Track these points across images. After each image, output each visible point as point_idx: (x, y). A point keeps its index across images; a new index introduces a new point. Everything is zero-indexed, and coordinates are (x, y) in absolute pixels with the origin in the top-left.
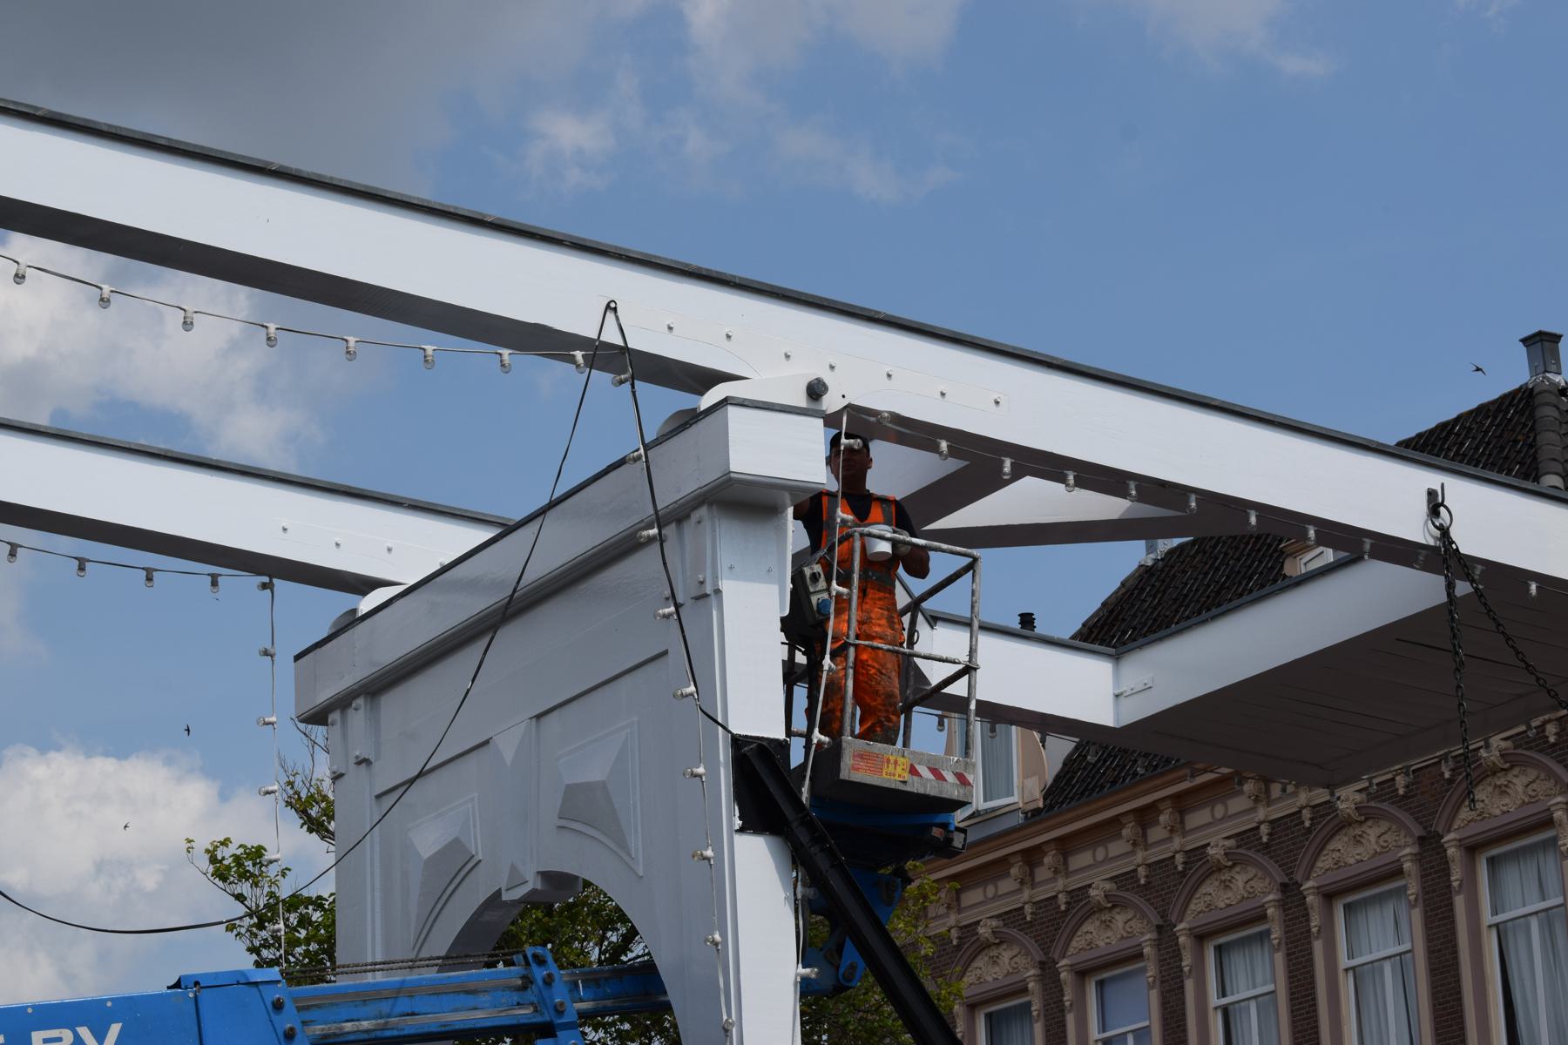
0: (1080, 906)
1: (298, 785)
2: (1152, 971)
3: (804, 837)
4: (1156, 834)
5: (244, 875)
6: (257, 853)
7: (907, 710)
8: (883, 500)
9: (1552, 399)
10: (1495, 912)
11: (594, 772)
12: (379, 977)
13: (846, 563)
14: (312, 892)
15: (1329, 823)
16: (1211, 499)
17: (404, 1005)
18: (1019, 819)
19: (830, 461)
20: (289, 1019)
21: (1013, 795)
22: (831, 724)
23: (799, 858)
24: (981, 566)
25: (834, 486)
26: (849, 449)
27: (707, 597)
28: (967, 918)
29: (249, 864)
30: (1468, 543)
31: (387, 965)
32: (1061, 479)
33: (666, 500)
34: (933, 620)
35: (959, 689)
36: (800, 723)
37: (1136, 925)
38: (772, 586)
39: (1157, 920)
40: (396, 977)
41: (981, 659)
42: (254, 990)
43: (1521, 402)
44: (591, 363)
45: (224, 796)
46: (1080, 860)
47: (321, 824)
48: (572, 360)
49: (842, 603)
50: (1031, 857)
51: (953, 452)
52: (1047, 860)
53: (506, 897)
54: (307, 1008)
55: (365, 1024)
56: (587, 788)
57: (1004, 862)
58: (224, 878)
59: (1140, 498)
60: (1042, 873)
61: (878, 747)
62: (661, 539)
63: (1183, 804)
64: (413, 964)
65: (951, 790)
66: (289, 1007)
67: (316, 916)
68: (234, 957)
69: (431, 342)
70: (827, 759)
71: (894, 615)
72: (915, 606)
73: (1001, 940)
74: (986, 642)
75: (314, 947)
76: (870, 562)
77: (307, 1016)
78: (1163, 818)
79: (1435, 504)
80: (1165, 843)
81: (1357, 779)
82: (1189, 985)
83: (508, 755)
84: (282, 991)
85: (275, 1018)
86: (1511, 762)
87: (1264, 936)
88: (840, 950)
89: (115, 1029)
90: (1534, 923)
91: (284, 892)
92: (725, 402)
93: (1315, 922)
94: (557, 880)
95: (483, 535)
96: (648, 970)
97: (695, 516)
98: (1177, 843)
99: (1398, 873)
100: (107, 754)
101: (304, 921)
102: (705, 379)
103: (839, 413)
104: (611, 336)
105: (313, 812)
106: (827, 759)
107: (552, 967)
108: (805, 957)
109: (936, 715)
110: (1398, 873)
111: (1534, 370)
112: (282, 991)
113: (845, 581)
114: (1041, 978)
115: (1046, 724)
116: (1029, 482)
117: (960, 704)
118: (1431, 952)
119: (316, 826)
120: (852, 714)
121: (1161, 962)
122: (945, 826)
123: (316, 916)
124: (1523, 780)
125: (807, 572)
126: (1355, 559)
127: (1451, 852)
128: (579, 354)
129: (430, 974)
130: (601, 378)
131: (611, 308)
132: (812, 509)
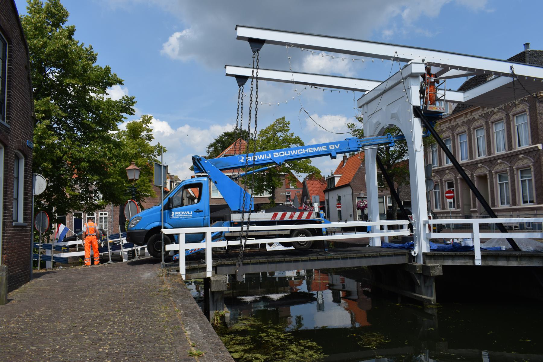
0: (457, 126)
1: (358, 116)
2: (467, 133)
3: (423, 118)
4: (468, 116)
5: (352, 127)
6: (353, 124)
7: (436, 101)
8: (433, 74)
9: (528, 53)
10: (517, 124)
11: (395, 111)
12: (369, 138)
13: (428, 83)
14: (360, 129)
15: (493, 113)
16: (479, 70)
17: (373, 141)
18: (449, 115)
19: (426, 69)
20: (359, 143)
22: (426, 103)
23: (422, 121)
24: (446, 82)
25: (426, 73)
26: (428, 68)
27: (409, 88)
28: (442, 128)
30: (516, 73)
31: (370, 136)
32: (457, 69)
33: (404, 76)
34: (439, 89)
35: (443, 98)
36: (422, 104)
37: (465, 128)
38: (417, 87)
39: (468, 127)
40: (371, 137)
41: (446, 94)
43: (523, 53)
44: (394, 60)
45: (348, 119)
46: (457, 120)
48: (391, 60)
49: (427, 88)
50: (451, 120)
51: (442, 67)
52: (453, 120)
53: (384, 127)
55: (368, 143)
56: (394, 114)
57: (447, 121)
59: (468, 71)
60: (452, 122)
61: (432, 106)
62: (403, 81)
63: (472, 112)
64: (373, 136)
65: (442, 111)
66: (359, 141)
67: (361, 131)
68: (351, 136)
69: (373, 59)
70: (426, 108)
71: (434, 88)
72: (437, 88)
73: (446, 131)
74: (447, 92)
76: (431, 83)
78: (469, 114)
79: (511, 68)
80: (469, 117)
81: (498, 106)
82: (472, 135)
83: (384, 110)
84: (358, 140)
86: (520, 103)
87: (483, 128)
88: (427, 131)
89: (339, 145)
90: (523, 125)
91: (357, 129)
92: (411, 63)
93: (490, 126)
94: (391, 125)
95: (380, 83)
96: (402, 136)
97: (408, 78)
98: (471, 117)
99: (503, 119)
101: (359, 132)
102: (408, 60)
103: (426, 63)
104: (396, 56)
105: (360, 119)
106: (426, 108)
107: (391, 135)
108: (423, 132)
109: (367, 137)
110: (503, 119)
111: (525, 49)
112: (358, 140)
113: (427, 85)
114: (452, 135)
115: (454, 102)
116: (452, 70)
117: (443, 100)
118: (507, 129)
119: (360, 121)
120: (429, 102)
121: (506, 119)
122: (441, 115)
123: (361, 131)
124: (522, 106)
125: (422, 84)
126: (499, 76)
127: (510, 116)
128: (392, 59)
129: (376, 137)
130: (395, 62)
131: (396, 52)
132: (423, 76)
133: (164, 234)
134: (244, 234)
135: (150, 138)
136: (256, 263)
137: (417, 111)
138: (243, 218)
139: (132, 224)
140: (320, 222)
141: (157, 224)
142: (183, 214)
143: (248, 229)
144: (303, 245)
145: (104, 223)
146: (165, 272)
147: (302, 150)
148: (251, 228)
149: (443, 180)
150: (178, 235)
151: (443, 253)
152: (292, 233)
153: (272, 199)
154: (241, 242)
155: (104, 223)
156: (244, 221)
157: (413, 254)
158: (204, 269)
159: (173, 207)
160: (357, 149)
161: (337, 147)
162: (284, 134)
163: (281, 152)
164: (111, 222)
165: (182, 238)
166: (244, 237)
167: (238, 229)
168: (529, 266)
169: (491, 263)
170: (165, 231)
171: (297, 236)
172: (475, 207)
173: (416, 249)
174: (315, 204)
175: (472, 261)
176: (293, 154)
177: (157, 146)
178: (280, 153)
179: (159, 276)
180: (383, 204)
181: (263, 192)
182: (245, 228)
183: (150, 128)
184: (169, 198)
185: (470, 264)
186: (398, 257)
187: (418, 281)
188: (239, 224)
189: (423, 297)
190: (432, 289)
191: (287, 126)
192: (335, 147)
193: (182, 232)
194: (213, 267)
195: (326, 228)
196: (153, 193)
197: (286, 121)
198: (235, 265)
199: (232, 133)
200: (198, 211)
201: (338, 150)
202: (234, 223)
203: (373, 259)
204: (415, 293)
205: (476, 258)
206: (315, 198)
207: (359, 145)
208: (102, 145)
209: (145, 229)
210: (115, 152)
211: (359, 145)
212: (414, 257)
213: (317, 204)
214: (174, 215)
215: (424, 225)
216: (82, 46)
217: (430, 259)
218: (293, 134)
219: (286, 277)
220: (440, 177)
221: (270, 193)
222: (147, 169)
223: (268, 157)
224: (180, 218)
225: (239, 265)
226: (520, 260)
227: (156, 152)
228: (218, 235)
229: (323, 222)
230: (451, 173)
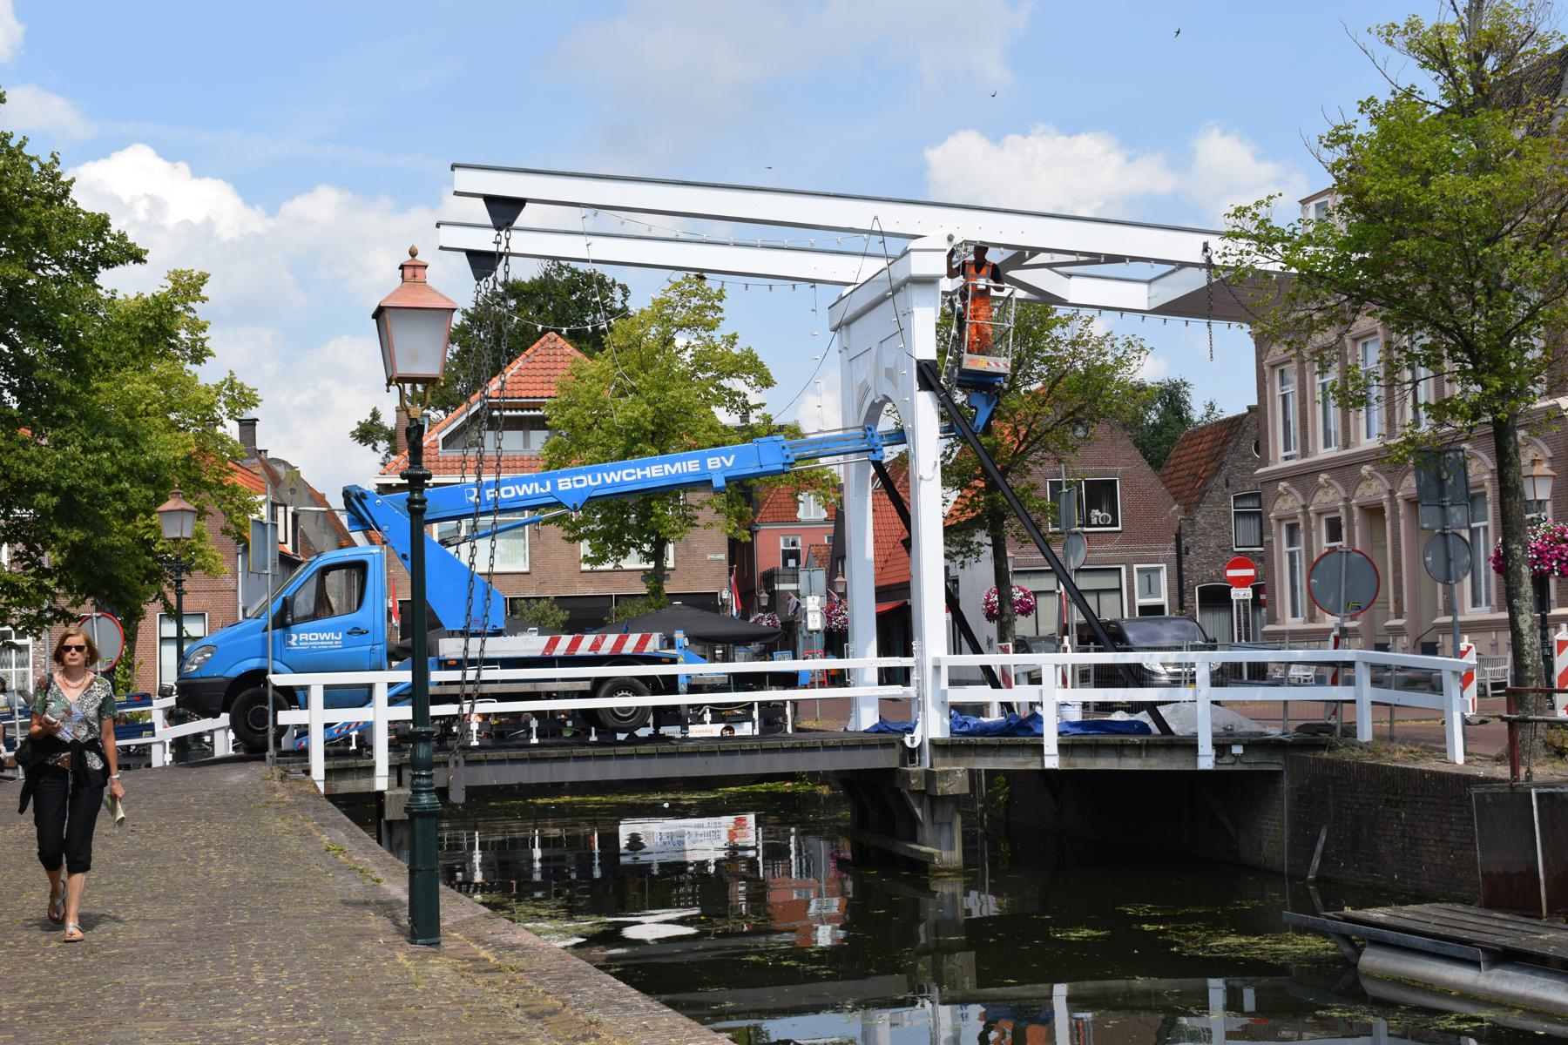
17: (824, 445)
20: (787, 452)
27: (908, 313)
89: (733, 457)
133: (275, 688)
134: (469, 689)
135: (199, 355)
136: (501, 761)
137: (927, 375)
138: (466, 649)
139: (193, 664)
140: (673, 661)
141: (254, 663)
142: (319, 640)
143: (478, 675)
144: (629, 718)
145: (14, 669)
146: (277, 772)
147: (633, 471)
148: (487, 674)
149: (1272, 515)
150: (306, 688)
151: (971, 739)
152: (598, 687)
153: (657, 576)
154: (461, 709)
155: (14, 669)
156: (470, 656)
157: (908, 744)
158: (370, 770)
159: (293, 623)
160: (780, 467)
161: (729, 464)
162: (699, 338)
163: (577, 475)
164: (44, 667)
165: (316, 697)
166: (468, 697)
167: (455, 675)
168: (1174, 768)
169: (1082, 763)
170: (278, 680)
171: (611, 694)
172: (1399, 615)
173: (918, 734)
174: (809, 599)
175: (1039, 759)
176: (609, 481)
177: (223, 384)
178: (575, 479)
179: (264, 779)
180: (1118, 596)
181: (625, 554)
182: (471, 674)
183: (202, 319)
184: (284, 599)
185: (1034, 765)
186: (874, 751)
187: (918, 811)
188: (459, 664)
189: (923, 849)
190: (951, 832)
191: (713, 307)
192: (722, 461)
193: (317, 682)
194: (391, 767)
195: (688, 677)
196: (215, 558)
197: (710, 289)
198: (446, 764)
199: (533, 283)
200: (357, 631)
201: (729, 469)
202: (446, 661)
203: (807, 755)
204: (915, 841)
205: (1047, 751)
206: (809, 578)
207: (787, 457)
208: (87, 440)
209: (226, 675)
210: (126, 458)
211: (787, 457)
212: (912, 752)
213: (817, 599)
214: (298, 641)
215: (937, 668)
216: (21, 146)
217: (943, 756)
218: (734, 337)
219: (685, 864)
220: (1305, 496)
221: (648, 557)
222: (189, 468)
223: (542, 490)
224: (310, 650)
225: (456, 763)
226: (1147, 756)
227: (221, 404)
228: (406, 692)
229: (681, 659)
230: (1377, 478)
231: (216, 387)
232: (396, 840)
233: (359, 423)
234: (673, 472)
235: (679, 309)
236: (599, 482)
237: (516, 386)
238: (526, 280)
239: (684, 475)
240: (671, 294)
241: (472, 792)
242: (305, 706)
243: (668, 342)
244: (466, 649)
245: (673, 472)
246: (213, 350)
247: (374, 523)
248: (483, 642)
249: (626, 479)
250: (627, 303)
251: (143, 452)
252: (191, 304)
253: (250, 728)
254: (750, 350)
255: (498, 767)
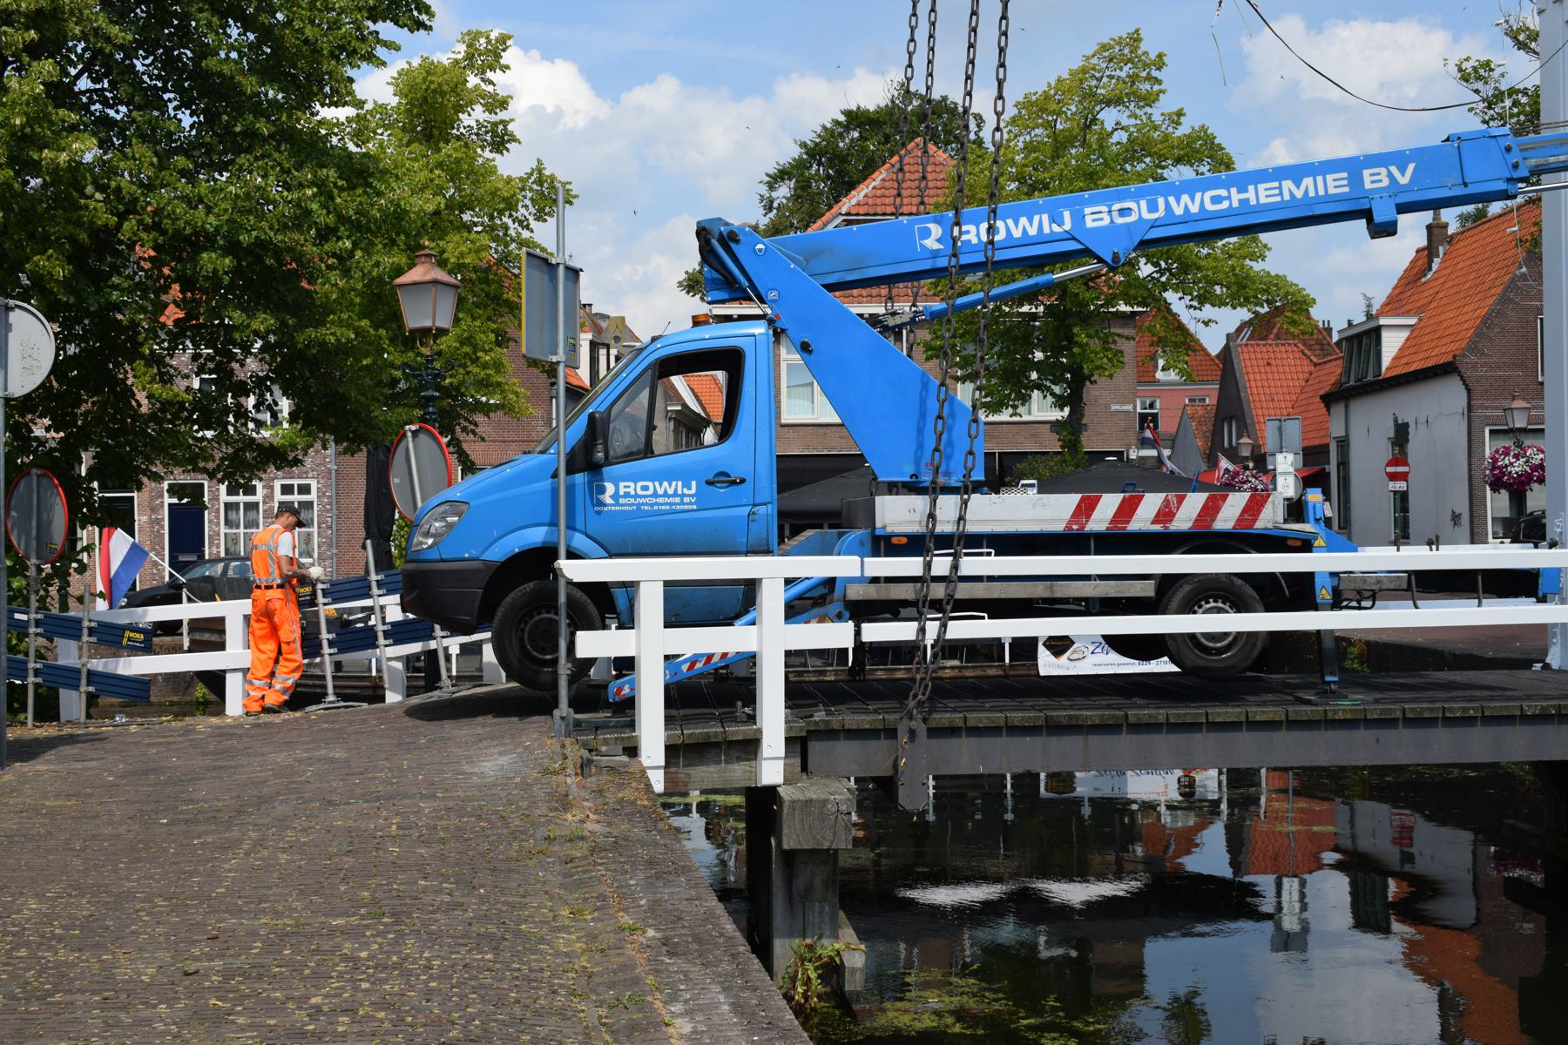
5: (1479, 78)
6: (1487, 65)
20: (1514, 157)
21: (221, 620)
29: (1482, 72)
42: (1493, 140)
47: (1526, 45)
54: (1527, 149)
58: (1466, 80)
66: (1515, 149)
67: (1524, 100)
75: (1522, 118)
77: (1526, 154)
85: (1507, 156)
89: (1411, 167)
100: (1385, 21)
101: (1516, 103)
105: (1521, 38)
123: (1524, 100)
133: (570, 583)
134: (938, 591)
135: (500, 140)
138: (932, 516)
139: (427, 534)
140: (1306, 546)
141: (536, 536)
142: (655, 495)
143: (955, 567)
144: (1220, 651)
145: (242, 530)
146: (575, 752)
147: (1223, 193)
148: (972, 565)
150: (631, 587)
153: (1070, 429)
158: (750, 747)
159: (608, 462)
160: (1502, 186)
163: (1120, 200)
165: (651, 605)
166: (937, 605)
167: (910, 566)
170: (575, 571)
171: (1188, 608)
174: (1280, 457)
178: (1116, 207)
179: (546, 772)
181: (1025, 399)
182: (941, 565)
183: (502, 93)
184: (591, 416)
188: (914, 545)
191: (1149, 78)
192: (1390, 175)
194: (788, 740)
196: (516, 394)
197: (1145, 53)
198: (892, 733)
199: (879, 111)
200: (722, 479)
201: (1405, 189)
202: (888, 538)
206: (1280, 429)
207: (1516, 166)
208: (288, 172)
211: (1516, 166)
213: (1290, 457)
214: (616, 496)
218: (1180, 114)
221: (1060, 402)
222: (487, 282)
223: (1056, 228)
224: (639, 512)
225: (912, 734)
227: (528, 202)
228: (816, 593)
229: (1319, 542)
231: (521, 179)
232: (799, 884)
233: (687, 273)
234: (1299, 194)
235: (1105, 80)
236: (1161, 213)
237: (879, 201)
238: (872, 108)
239: (1319, 200)
240: (1094, 61)
241: (953, 790)
242: (627, 621)
243: (1090, 122)
244: (932, 516)
245: (1299, 194)
246: (518, 135)
247: (752, 285)
248: (965, 503)
249: (1209, 207)
250: (981, 134)
251: (379, 194)
252: (490, 75)
253: (529, 656)
254: (1203, 128)
255: (987, 741)
